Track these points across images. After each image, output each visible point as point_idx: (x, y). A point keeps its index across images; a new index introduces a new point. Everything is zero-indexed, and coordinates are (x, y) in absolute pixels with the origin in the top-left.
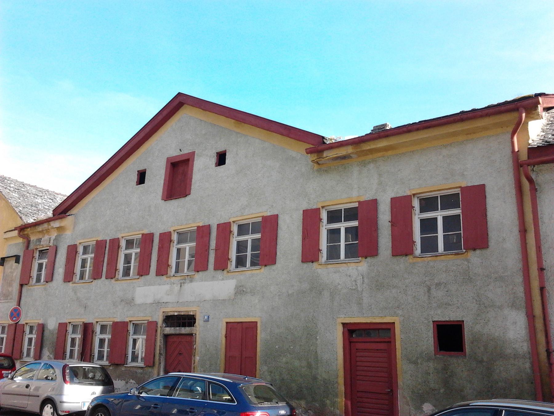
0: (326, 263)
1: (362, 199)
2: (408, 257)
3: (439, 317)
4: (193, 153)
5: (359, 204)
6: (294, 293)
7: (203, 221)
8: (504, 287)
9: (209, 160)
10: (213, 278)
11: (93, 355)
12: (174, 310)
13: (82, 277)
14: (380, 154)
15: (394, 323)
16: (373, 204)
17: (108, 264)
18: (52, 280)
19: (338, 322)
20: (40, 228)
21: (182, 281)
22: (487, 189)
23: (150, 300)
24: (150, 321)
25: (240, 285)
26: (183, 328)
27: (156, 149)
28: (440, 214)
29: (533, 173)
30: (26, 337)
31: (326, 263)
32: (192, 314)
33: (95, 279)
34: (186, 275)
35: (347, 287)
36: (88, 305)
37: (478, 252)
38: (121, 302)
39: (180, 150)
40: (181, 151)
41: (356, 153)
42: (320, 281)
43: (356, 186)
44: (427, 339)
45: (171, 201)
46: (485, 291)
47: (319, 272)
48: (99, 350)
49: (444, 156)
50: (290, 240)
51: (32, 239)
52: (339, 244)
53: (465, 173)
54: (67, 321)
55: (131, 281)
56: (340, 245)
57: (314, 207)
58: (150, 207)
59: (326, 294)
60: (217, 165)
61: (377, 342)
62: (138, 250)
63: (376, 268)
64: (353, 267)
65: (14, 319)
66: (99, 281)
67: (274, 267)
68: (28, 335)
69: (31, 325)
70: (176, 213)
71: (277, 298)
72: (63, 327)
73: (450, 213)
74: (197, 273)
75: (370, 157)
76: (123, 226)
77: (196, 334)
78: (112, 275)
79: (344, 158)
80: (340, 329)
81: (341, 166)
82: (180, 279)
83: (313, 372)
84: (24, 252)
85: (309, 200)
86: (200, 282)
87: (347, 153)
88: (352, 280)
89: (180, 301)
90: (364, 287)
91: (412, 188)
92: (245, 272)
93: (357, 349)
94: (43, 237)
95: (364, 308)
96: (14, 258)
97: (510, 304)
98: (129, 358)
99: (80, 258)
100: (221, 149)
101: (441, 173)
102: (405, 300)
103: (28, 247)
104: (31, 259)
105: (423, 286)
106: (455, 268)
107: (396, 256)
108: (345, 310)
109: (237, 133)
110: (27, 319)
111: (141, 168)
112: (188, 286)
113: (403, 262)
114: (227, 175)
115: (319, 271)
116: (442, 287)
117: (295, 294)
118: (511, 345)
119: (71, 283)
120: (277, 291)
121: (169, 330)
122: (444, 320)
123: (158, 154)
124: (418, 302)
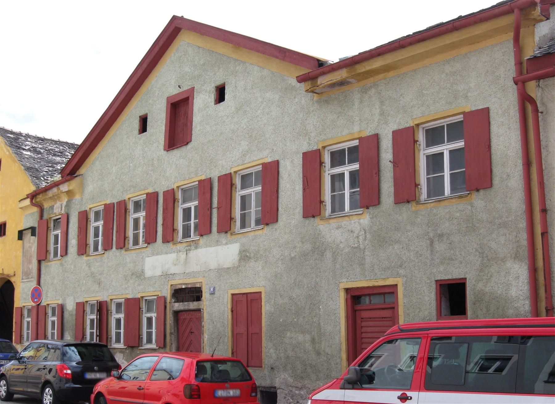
0: (330, 217)
1: (364, 135)
2: (410, 204)
3: (442, 276)
4: (193, 89)
5: (464, 117)
6: (296, 256)
7: (205, 174)
8: (507, 235)
9: (208, 96)
10: (218, 243)
11: (110, 338)
12: (181, 282)
13: (136, 242)
14: (381, 76)
15: (397, 285)
16: (376, 139)
17: (117, 232)
18: (66, 253)
19: (340, 288)
20: (50, 193)
21: (187, 248)
22: (492, 114)
23: (158, 273)
24: (159, 296)
25: (243, 249)
26: (191, 303)
27: (156, 87)
28: (446, 148)
29: (538, 90)
30: (87, 319)
31: (330, 217)
32: (198, 286)
33: (106, 250)
34: (190, 241)
35: (349, 245)
36: (101, 281)
37: (482, 192)
38: (132, 275)
39: (179, 86)
40: (180, 88)
41: (353, 77)
42: (322, 240)
43: (357, 119)
44: (429, 302)
45: (173, 150)
46: (489, 241)
47: (321, 229)
48: (116, 332)
49: (447, 74)
50: (291, 191)
51: (45, 207)
52: (443, 174)
53: (469, 94)
54: (84, 300)
55: (140, 250)
56: (444, 175)
57: (315, 147)
58: (153, 159)
59: (328, 254)
60: (218, 102)
61: (383, 309)
62: (259, 188)
63: (378, 220)
64: (356, 220)
65: (36, 300)
66: (111, 252)
67: (276, 226)
68: (50, 317)
69: (53, 306)
70: (178, 165)
71: (280, 262)
72: (81, 307)
73: (456, 145)
74: (476, 193)
75: (371, 80)
76: (129, 185)
77: (203, 309)
78: (122, 245)
79: (342, 83)
80: (342, 295)
81: (342, 93)
82: (185, 245)
83: (317, 347)
84: (39, 222)
85: (309, 139)
86: (205, 248)
87: (342, 78)
88: (355, 236)
89: (187, 272)
90: (366, 244)
91: (415, 117)
92: (248, 233)
93: (362, 318)
94: (56, 203)
95: (366, 269)
96: (30, 231)
97: (513, 256)
98: (143, 339)
99: (180, 208)
100: (219, 83)
101: (445, 96)
102: (407, 257)
103: (41, 216)
104: (413, 144)
105: (426, 239)
106: (458, 214)
107: (399, 203)
108: (348, 273)
109: (236, 60)
110: (48, 300)
111: (142, 113)
112: (193, 254)
113: (407, 210)
114: (226, 114)
115: (321, 227)
116: (445, 238)
117: (297, 257)
118: (513, 304)
119: (85, 255)
120: (280, 254)
121: (178, 306)
122: (446, 278)
123: (158, 94)
124: (421, 258)
